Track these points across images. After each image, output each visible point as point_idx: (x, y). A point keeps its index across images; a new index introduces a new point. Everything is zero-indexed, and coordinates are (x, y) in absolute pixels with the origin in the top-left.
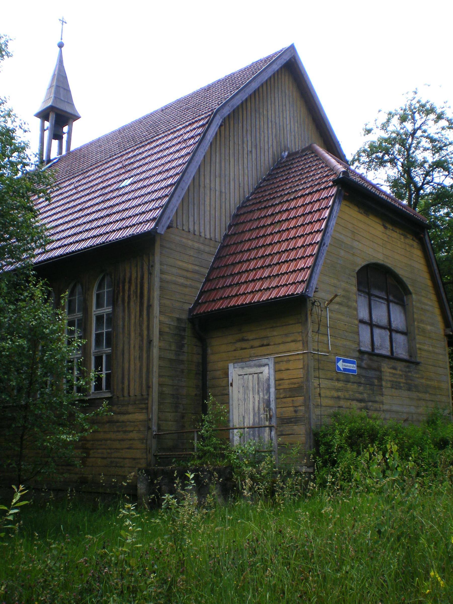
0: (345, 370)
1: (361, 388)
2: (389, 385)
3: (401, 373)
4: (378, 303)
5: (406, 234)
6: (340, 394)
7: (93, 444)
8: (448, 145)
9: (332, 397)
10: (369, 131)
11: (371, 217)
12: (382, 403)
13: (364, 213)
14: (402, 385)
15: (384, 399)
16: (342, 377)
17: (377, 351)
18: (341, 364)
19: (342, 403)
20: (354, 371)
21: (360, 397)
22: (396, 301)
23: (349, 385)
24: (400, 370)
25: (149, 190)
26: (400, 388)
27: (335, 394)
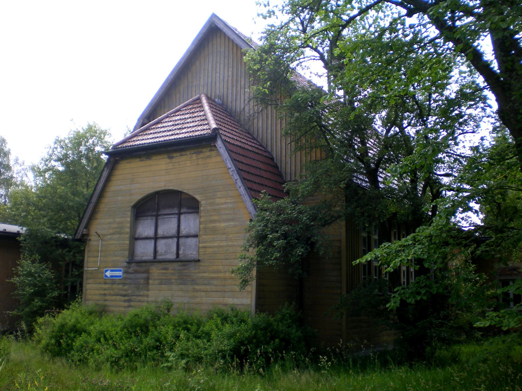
0: (111, 276)
1: (126, 287)
2: (157, 282)
3: (173, 272)
4: (167, 219)
5: (200, 150)
6: (106, 292)
7: (39, 342)
8: (290, 21)
9: (100, 295)
10: (271, 13)
11: (154, 158)
12: (147, 296)
13: (146, 158)
14: (173, 281)
15: (150, 293)
16: (108, 281)
17: (159, 257)
18: (108, 274)
19: (107, 298)
20: (120, 276)
21: (124, 293)
22: (190, 211)
23: (114, 286)
24: (172, 270)
25: (166, 129)
26: (172, 283)
27: (103, 292)
